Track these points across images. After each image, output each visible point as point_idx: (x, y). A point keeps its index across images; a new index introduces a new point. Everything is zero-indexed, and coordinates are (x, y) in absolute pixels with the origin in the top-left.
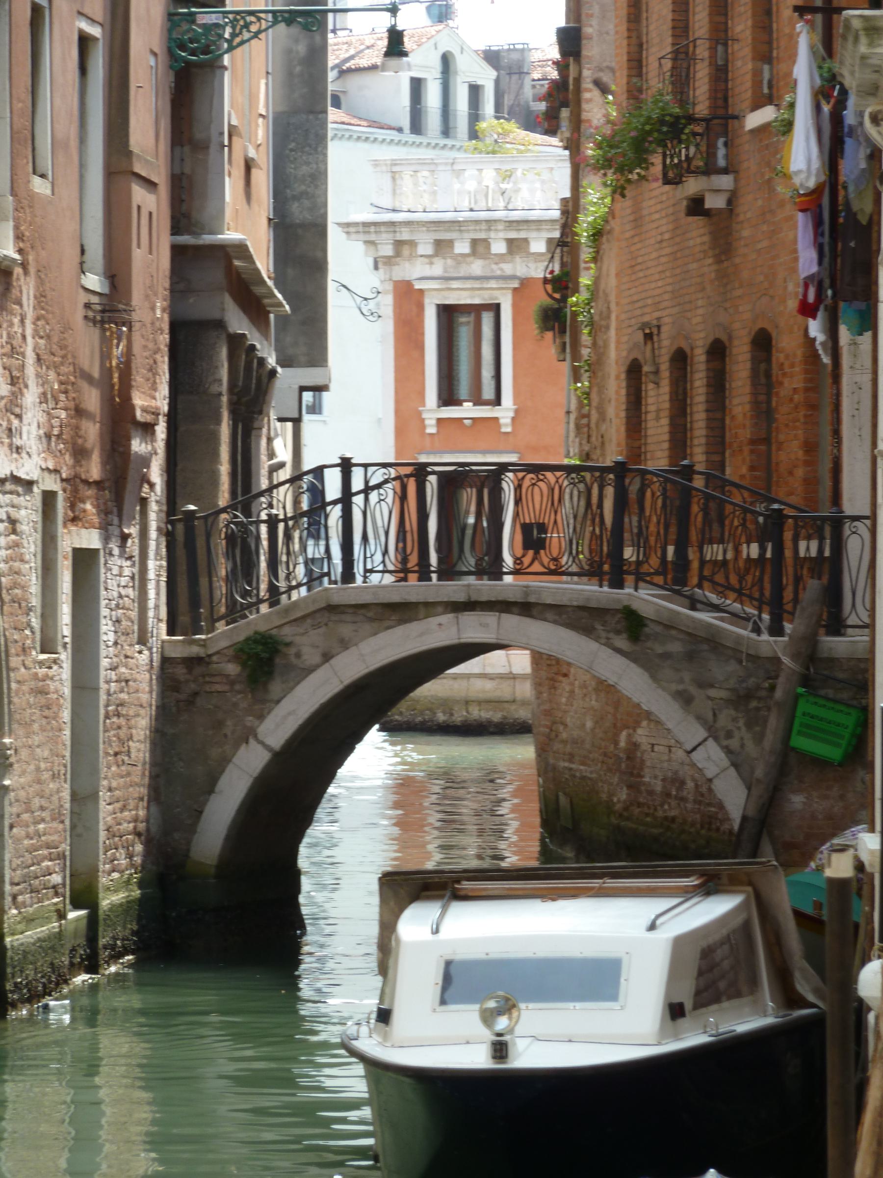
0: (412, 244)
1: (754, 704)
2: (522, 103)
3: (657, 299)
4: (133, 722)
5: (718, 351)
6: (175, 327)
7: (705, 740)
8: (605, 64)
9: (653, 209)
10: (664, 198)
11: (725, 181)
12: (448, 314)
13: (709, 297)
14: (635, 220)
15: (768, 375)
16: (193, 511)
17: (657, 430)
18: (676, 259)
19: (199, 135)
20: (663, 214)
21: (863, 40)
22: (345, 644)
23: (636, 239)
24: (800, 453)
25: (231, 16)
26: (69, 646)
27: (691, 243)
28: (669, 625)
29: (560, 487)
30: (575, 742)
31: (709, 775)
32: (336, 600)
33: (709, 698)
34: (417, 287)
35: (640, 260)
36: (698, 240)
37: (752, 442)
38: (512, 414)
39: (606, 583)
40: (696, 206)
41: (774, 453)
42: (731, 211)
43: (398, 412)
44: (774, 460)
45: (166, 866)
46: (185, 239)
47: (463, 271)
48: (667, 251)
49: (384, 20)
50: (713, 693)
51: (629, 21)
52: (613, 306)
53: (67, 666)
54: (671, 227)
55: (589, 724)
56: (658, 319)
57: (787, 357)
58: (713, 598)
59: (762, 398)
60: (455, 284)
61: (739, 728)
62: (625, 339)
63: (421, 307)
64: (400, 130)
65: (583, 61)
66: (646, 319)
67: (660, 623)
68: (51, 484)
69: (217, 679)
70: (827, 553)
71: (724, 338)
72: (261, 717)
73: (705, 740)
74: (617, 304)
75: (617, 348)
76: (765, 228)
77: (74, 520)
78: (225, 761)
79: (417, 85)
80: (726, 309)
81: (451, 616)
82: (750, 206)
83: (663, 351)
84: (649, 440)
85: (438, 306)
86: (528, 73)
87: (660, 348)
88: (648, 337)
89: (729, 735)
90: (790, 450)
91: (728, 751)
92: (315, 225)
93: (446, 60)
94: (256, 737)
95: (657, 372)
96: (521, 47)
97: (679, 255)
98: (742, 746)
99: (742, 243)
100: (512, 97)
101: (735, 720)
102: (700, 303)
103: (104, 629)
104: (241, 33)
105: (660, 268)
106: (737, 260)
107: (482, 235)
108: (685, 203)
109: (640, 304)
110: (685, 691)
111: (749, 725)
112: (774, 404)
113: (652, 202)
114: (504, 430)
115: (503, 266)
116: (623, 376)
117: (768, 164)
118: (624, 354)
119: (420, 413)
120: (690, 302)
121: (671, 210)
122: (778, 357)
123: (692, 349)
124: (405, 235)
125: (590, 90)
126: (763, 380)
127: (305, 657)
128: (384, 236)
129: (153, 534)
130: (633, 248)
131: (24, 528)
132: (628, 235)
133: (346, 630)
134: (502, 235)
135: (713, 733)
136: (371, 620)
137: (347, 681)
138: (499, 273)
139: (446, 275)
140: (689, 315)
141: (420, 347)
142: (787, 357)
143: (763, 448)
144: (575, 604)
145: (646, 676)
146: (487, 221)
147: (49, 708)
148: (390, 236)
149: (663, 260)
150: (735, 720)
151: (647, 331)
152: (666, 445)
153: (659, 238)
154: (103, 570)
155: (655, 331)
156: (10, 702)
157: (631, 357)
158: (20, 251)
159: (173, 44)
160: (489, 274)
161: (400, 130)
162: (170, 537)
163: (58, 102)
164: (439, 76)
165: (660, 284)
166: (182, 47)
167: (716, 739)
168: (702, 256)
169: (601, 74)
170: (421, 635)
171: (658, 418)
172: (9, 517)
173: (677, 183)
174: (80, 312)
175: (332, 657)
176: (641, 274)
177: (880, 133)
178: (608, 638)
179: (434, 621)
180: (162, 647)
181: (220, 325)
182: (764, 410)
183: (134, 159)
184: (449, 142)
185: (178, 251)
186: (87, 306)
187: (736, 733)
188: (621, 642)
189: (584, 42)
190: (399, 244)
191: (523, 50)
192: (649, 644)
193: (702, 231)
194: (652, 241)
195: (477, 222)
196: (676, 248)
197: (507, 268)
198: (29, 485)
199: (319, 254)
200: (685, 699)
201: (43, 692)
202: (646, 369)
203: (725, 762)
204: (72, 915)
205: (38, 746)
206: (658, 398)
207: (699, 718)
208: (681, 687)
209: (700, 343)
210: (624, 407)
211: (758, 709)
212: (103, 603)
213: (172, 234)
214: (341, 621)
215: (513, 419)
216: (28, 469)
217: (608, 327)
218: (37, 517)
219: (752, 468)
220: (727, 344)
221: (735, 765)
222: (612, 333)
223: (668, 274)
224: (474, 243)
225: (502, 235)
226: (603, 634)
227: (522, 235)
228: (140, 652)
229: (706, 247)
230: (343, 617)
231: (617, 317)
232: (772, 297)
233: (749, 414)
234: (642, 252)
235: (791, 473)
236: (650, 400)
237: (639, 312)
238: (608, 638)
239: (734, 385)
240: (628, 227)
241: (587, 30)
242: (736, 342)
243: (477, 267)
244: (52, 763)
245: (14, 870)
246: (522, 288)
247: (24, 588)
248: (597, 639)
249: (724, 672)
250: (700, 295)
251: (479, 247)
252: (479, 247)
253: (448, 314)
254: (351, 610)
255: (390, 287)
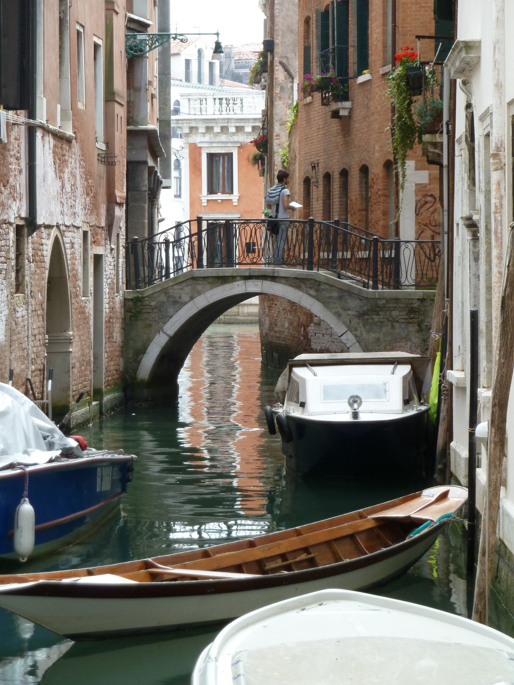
0: (196, 128)
1: (366, 317)
2: (231, 70)
3: (317, 152)
4: (114, 325)
5: (344, 174)
6: (129, 163)
7: (346, 332)
8: (284, 55)
9: (315, 115)
10: (320, 111)
11: (347, 104)
12: (211, 157)
13: (340, 152)
14: (307, 120)
15: (367, 183)
16: (137, 239)
17: (317, 206)
18: (325, 136)
19: (136, 85)
20: (320, 117)
21: (464, 51)
22: (199, 293)
23: (308, 128)
24: (381, 215)
25: (151, 36)
26: (93, 294)
27: (332, 129)
28: (331, 285)
29: (255, 229)
30: (280, 332)
31: (348, 346)
32: (196, 275)
33: (348, 314)
34: (198, 146)
35: (309, 136)
36: (336, 128)
37: (360, 210)
38: (238, 198)
39: (305, 268)
40: (335, 114)
41: (369, 215)
42: (350, 116)
43: (190, 197)
44: (370, 218)
45: (127, 382)
46: (131, 127)
47: (218, 139)
48: (322, 132)
49: (215, 38)
50: (349, 312)
51: (304, 38)
52: (297, 155)
53: (92, 302)
54: (323, 123)
55: (287, 325)
56: (318, 160)
57: (375, 175)
58: (349, 274)
59: (364, 193)
60: (214, 145)
61: (360, 327)
62: (303, 168)
63: (200, 154)
64: (181, 81)
65: (275, 54)
66: (312, 160)
67: (327, 284)
68: (86, 228)
69: (148, 307)
70: (393, 256)
71: (347, 168)
72: (165, 323)
73: (346, 332)
74: (299, 154)
75: (299, 172)
76: (365, 123)
77: (94, 242)
78: (149, 340)
79: (188, 62)
80: (348, 156)
81: (243, 281)
82: (358, 115)
83: (320, 173)
84: (314, 209)
85: (207, 153)
86: (233, 57)
87: (318, 172)
88: (313, 167)
89: (356, 330)
90: (376, 214)
91: (356, 336)
92: (165, 121)
93: (200, 52)
94: (163, 331)
95: (317, 182)
96: (230, 46)
97: (327, 134)
98: (362, 334)
99: (355, 129)
100: (227, 67)
101: (358, 323)
102: (336, 154)
103: (104, 287)
104: (155, 43)
105: (318, 140)
106: (353, 137)
107: (226, 125)
108: (330, 113)
109: (309, 154)
110: (338, 312)
111: (364, 326)
112: (370, 195)
113: (315, 112)
114: (234, 204)
115: (234, 137)
116: (302, 183)
117: (367, 97)
118: (303, 174)
119: (200, 197)
120: (332, 153)
121: (323, 116)
122: (371, 176)
123: (333, 173)
124: (193, 125)
125: (278, 66)
126: (364, 186)
127: (183, 298)
128: (185, 125)
129: (121, 248)
130: (306, 131)
131: (76, 246)
132: (304, 126)
133: (199, 287)
134: (233, 124)
135: (350, 329)
136: (209, 283)
137: (200, 308)
138: (232, 140)
139: (211, 141)
140: (331, 159)
141: (200, 170)
142: (375, 175)
143: (364, 213)
144: (293, 276)
145: (322, 306)
146: (227, 119)
147: (86, 319)
148: (188, 125)
149: (320, 136)
150: (358, 323)
151: (313, 165)
152: (321, 212)
153: (318, 127)
154: (104, 263)
155: (316, 165)
156: (72, 317)
157: (306, 176)
158: (74, 133)
159: (128, 48)
160: (228, 141)
161: (181, 81)
162: (127, 248)
163: (87, 71)
164: (197, 58)
165: (318, 146)
166: (131, 49)
167: (351, 331)
168: (337, 134)
169: (282, 59)
170: (231, 289)
171: (317, 201)
172: (71, 242)
173: (327, 105)
174: (96, 157)
175: (194, 298)
176: (310, 142)
177: (466, 88)
178: (307, 291)
179: (236, 283)
180: (124, 294)
181: (146, 163)
182: (366, 199)
183: (116, 95)
184: (201, 86)
185: (130, 133)
186: (99, 155)
187: (359, 329)
188: (312, 292)
189: (275, 46)
190: (191, 128)
191: (231, 48)
192: (324, 293)
193: (337, 125)
194: (315, 128)
195: (224, 119)
196: (325, 131)
197: (236, 138)
198: (78, 228)
199: (167, 133)
200: (338, 315)
201: (83, 313)
202: (313, 180)
203: (355, 341)
204: (94, 403)
205: (82, 335)
206: (317, 193)
207: (344, 323)
208: (336, 310)
209: (336, 170)
210: (302, 196)
211: (368, 319)
212: (104, 276)
213: (127, 125)
214: (198, 284)
215: (238, 200)
216: (78, 222)
217: (295, 164)
218: (81, 241)
219: (360, 221)
220: (348, 171)
221: (359, 342)
222: (297, 165)
223: (322, 142)
224: (222, 128)
225: (233, 124)
226: (305, 289)
227: (242, 124)
228: (117, 296)
229: (339, 131)
230: (199, 282)
231: (299, 159)
232: (368, 152)
233: (358, 199)
234: (311, 133)
235: (377, 223)
236: (314, 193)
237: (309, 157)
238: (307, 291)
239: (351, 187)
240: (304, 122)
241: (277, 41)
242: (352, 170)
243: (223, 138)
244: (87, 342)
245: (73, 386)
246: (241, 147)
247: (77, 271)
248: (302, 291)
249: (353, 303)
250: (337, 151)
251: (224, 129)
252: (224, 129)
253: (211, 157)
254: (202, 279)
255: (187, 145)
